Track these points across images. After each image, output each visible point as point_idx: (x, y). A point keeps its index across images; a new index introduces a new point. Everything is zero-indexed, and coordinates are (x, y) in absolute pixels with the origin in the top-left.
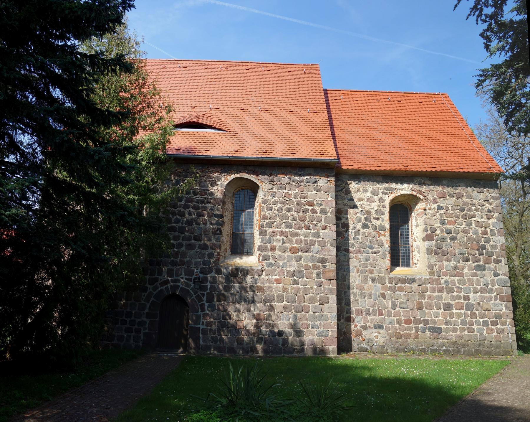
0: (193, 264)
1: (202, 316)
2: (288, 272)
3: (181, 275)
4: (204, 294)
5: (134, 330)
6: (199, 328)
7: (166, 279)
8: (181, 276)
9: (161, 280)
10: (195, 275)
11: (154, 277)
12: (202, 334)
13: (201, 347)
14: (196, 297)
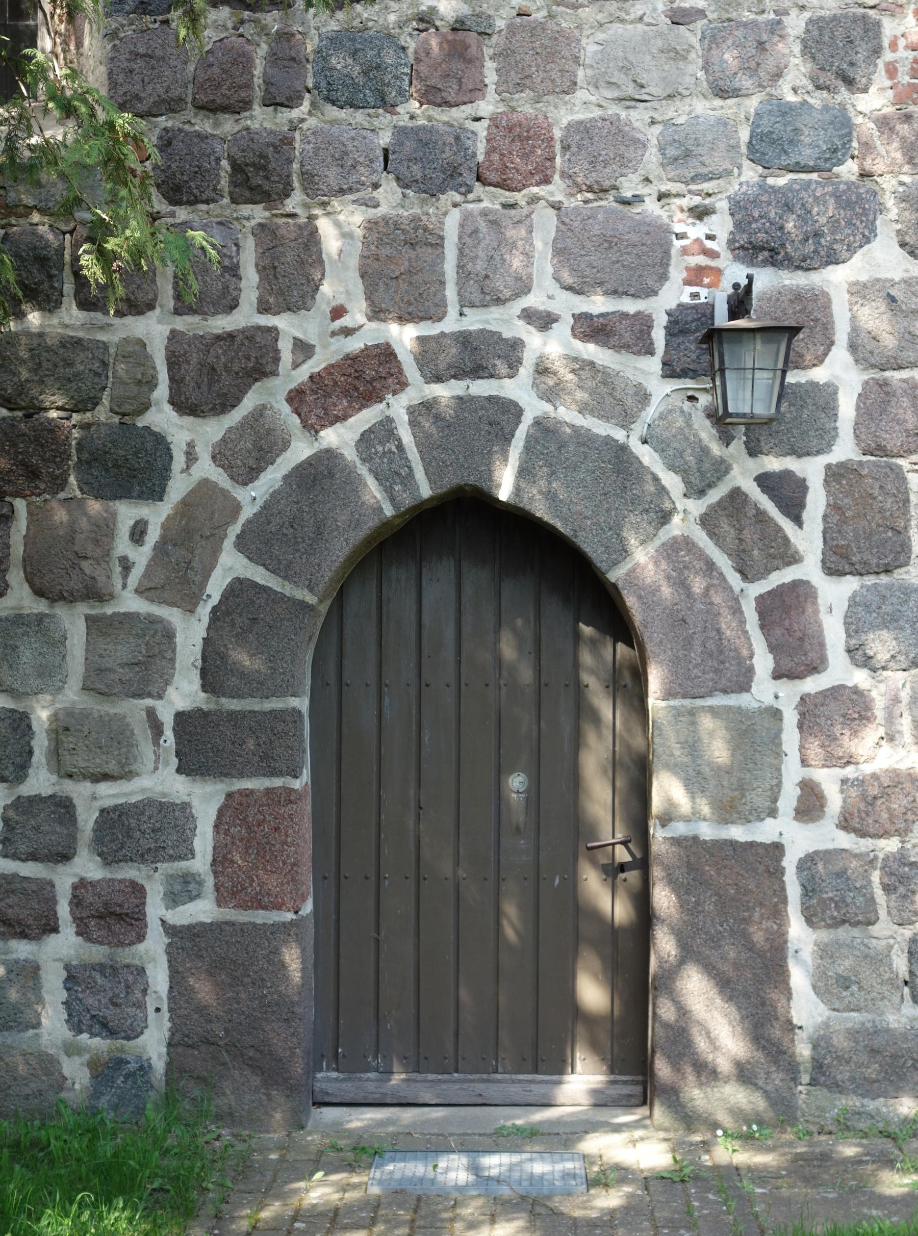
0: (652, 156)
1: (791, 718)
2: (800, 242)
3: (526, 289)
4: (801, 486)
5: (64, 910)
6: (777, 849)
7: (354, 345)
8: (529, 301)
9: (303, 349)
10: (677, 274)
11: (222, 324)
12: (810, 920)
13: (803, 1051)
14: (706, 521)
